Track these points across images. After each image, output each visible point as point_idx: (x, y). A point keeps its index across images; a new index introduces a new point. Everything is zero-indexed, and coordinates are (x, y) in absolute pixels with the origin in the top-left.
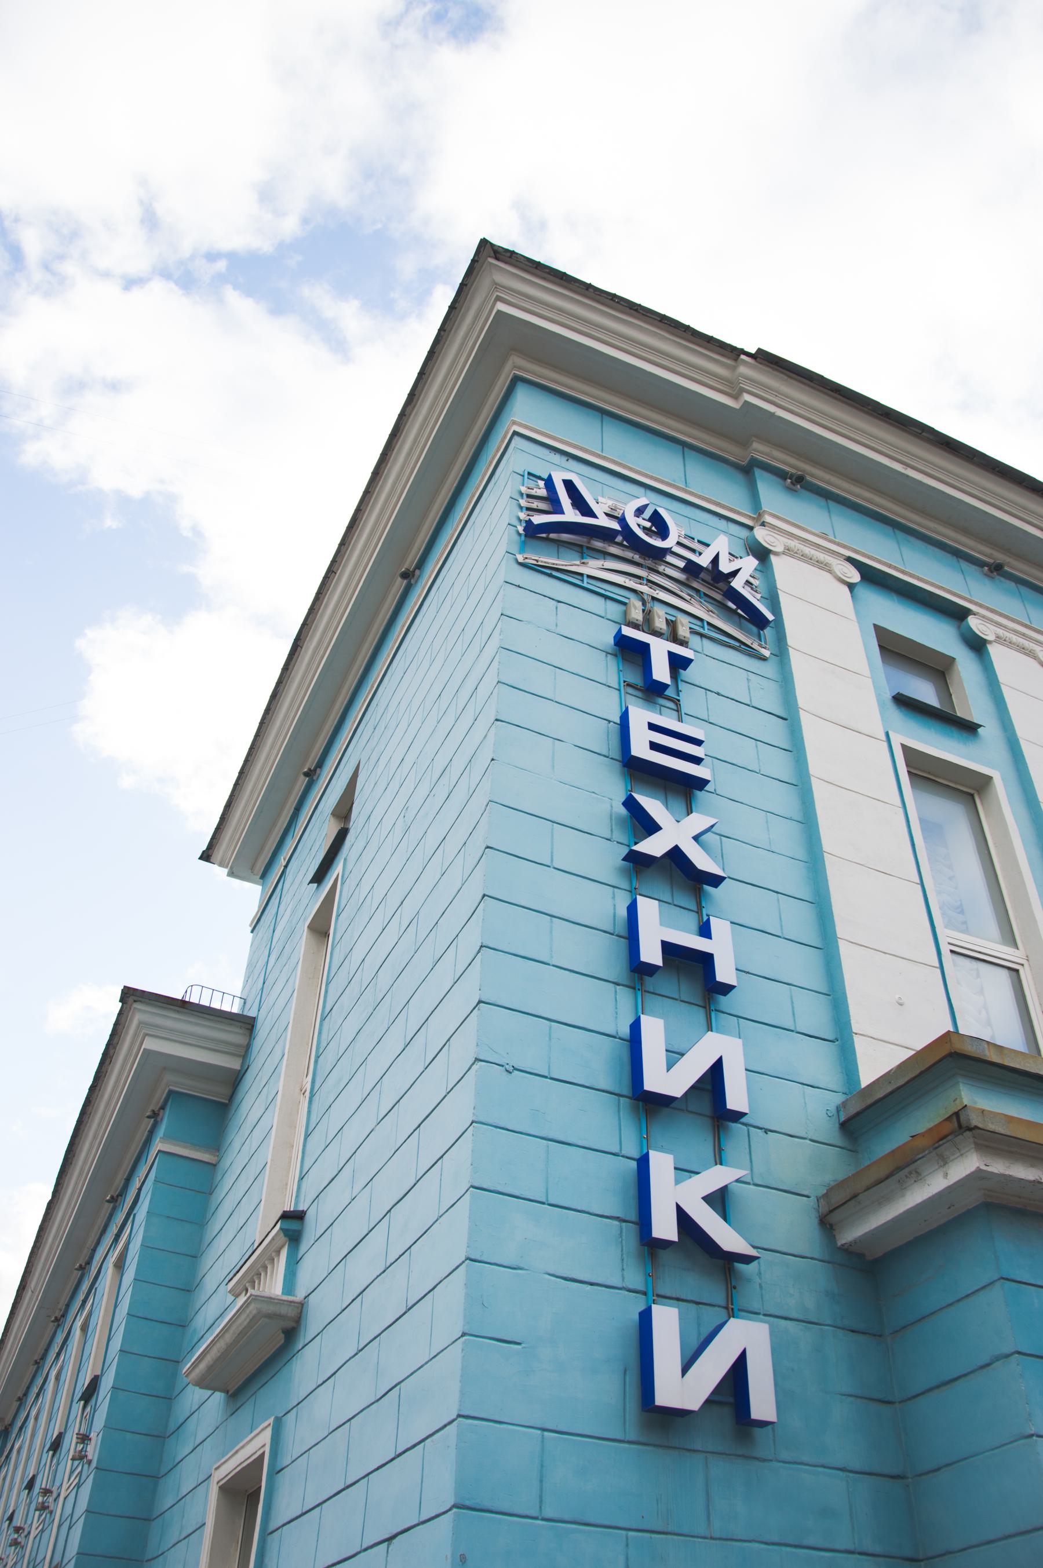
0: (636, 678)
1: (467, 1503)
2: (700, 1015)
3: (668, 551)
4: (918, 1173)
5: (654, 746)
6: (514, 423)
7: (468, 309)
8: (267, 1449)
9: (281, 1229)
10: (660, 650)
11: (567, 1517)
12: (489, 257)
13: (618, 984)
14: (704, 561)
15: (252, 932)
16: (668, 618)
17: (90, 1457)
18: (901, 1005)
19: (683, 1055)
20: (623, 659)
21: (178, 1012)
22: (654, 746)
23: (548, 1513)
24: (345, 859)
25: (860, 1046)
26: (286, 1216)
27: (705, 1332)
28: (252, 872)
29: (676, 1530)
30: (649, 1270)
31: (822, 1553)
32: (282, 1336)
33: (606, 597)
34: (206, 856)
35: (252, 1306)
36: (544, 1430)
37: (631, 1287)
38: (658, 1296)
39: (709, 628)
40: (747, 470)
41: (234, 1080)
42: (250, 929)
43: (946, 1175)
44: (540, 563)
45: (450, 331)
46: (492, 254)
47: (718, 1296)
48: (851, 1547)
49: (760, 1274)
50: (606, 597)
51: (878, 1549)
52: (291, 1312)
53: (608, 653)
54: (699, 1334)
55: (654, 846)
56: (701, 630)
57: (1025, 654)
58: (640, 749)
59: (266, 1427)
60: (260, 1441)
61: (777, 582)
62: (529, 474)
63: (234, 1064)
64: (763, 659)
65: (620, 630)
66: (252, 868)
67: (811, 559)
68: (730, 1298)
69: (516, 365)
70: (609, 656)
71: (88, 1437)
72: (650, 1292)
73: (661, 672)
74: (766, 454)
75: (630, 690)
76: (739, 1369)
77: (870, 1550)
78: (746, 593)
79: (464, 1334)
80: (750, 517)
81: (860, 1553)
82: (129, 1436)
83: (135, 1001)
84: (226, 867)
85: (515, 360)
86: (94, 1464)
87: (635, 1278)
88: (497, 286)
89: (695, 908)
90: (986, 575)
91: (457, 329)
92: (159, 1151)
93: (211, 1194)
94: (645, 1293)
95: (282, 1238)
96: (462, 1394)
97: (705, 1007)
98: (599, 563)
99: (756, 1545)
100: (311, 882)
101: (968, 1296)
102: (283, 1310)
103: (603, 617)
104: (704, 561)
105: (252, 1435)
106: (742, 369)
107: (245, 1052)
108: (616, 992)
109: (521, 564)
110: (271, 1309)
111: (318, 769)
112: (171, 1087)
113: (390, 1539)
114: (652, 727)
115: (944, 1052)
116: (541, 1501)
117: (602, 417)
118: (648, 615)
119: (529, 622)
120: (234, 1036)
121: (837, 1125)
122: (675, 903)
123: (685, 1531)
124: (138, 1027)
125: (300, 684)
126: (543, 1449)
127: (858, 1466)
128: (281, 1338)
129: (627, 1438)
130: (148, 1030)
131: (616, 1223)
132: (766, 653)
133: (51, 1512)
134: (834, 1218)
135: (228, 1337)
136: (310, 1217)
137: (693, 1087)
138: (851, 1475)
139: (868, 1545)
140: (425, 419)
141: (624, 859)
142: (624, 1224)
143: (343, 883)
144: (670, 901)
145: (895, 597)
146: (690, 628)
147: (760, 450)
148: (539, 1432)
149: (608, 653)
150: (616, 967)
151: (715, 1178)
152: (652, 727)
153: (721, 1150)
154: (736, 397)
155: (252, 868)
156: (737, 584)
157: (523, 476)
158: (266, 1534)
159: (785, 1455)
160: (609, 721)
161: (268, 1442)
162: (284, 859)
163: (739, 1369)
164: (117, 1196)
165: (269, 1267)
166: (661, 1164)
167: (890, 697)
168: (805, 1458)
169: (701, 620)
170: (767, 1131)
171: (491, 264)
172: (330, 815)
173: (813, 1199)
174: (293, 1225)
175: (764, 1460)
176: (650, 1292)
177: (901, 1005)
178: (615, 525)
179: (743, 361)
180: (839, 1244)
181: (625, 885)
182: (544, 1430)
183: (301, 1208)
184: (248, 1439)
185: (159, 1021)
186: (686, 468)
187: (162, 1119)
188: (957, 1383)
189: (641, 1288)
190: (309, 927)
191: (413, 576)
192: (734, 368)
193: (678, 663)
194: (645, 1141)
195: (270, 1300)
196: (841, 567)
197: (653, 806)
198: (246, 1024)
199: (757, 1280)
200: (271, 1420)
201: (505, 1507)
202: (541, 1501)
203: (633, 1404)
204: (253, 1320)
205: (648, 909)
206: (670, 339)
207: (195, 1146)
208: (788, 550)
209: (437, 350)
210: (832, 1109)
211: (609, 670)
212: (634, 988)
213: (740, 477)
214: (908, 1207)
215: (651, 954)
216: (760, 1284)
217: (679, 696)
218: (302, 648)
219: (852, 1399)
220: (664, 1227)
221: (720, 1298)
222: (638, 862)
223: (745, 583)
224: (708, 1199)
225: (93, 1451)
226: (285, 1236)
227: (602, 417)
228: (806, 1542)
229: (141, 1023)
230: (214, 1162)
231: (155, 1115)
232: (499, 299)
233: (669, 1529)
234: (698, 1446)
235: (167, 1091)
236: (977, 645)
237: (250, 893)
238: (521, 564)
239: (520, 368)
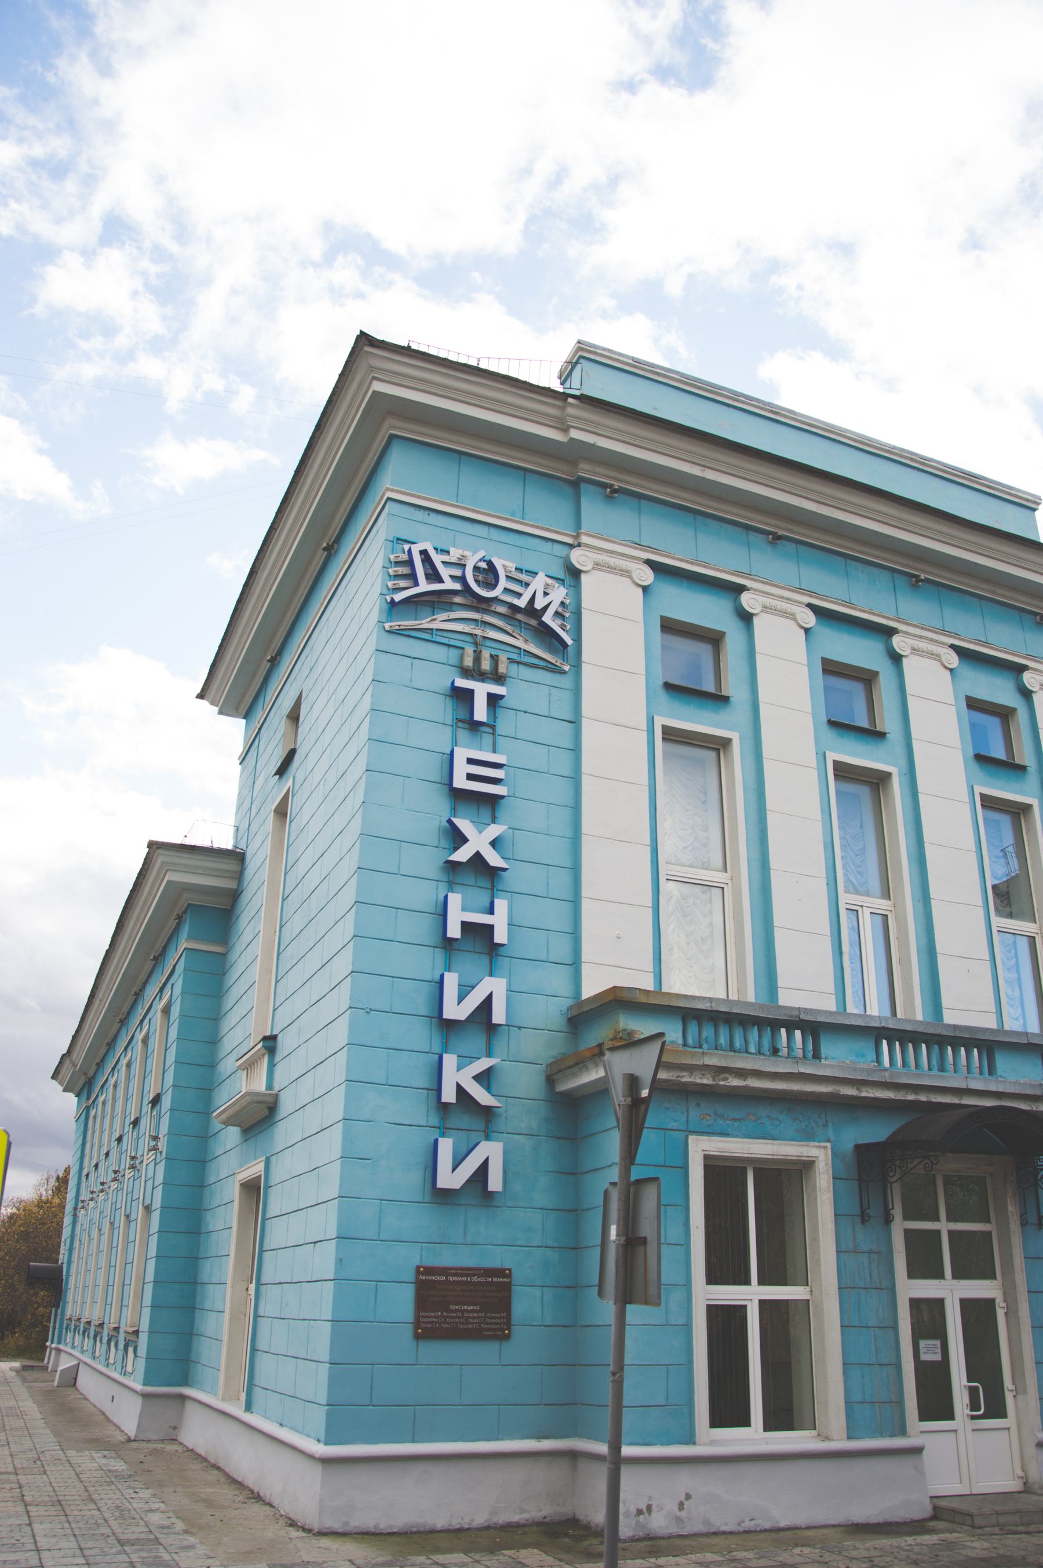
0: (463, 715)
1: (343, 1236)
2: (485, 959)
3: (495, 599)
4: (587, 1068)
5: (470, 777)
6: (388, 489)
7: (353, 379)
8: (263, 1173)
9: (263, 1046)
10: (481, 690)
11: (392, 1239)
12: (366, 345)
13: (436, 947)
14: (522, 603)
15: (241, 764)
16: (493, 653)
17: (161, 1150)
18: (619, 938)
19: (473, 987)
20: (457, 698)
21: (189, 853)
22: (470, 777)
23: (382, 1237)
24: (294, 777)
25: (586, 970)
26: (265, 1039)
27: (471, 1145)
28: (237, 712)
29: (447, 1242)
30: (442, 1116)
31: (524, 1248)
32: (267, 1110)
33: (449, 646)
34: (201, 696)
35: (248, 1097)
36: (382, 1200)
37: (432, 1125)
38: (446, 1128)
39: (525, 653)
40: (576, 484)
41: (234, 896)
42: (238, 762)
43: (597, 1072)
44: (402, 627)
45: (342, 388)
46: (367, 343)
47: (481, 1126)
48: (541, 1244)
49: (506, 1111)
50: (449, 646)
51: (555, 1245)
52: (271, 1100)
53: (446, 695)
54: (468, 1147)
55: (463, 855)
56: (519, 659)
57: (787, 617)
58: (460, 782)
59: (261, 1162)
60: (257, 1168)
61: (583, 602)
62: (398, 539)
63: (231, 885)
64: (564, 672)
65: (453, 683)
66: (237, 709)
67: (615, 569)
68: (487, 1127)
69: (392, 426)
70: (447, 697)
71: (157, 1137)
72: (442, 1128)
73: (481, 713)
74: (590, 471)
75: (460, 724)
76: (484, 1166)
77: (551, 1245)
78: (555, 625)
79: (341, 1158)
80: (571, 535)
81: (545, 1247)
82: (184, 1138)
83: (158, 848)
84: (217, 706)
85: (391, 421)
86: (164, 1155)
87: (434, 1120)
88: (372, 368)
89: (490, 886)
90: (770, 542)
91: (347, 390)
92: (185, 949)
93: (224, 975)
94: (439, 1128)
95: (264, 1051)
96: (341, 1186)
97: (489, 954)
98: (444, 616)
99: (489, 1246)
100: (275, 774)
101: (608, 1130)
102: (267, 1099)
103: (445, 664)
104: (522, 603)
105: (254, 1163)
106: (570, 410)
107: (240, 876)
108: (434, 953)
109: (388, 631)
110: (259, 1098)
111: (278, 657)
112: (189, 902)
113: (315, 1243)
114: (471, 761)
115: (611, 998)
116: (379, 1233)
117: (460, 458)
118: (477, 659)
119: (392, 683)
120: (232, 866)
121: (566, 1019)
122: (478, 885)
123: (452, 1242)
124: (162, 864)
125: (258, 597)
126: (381, 1209)
127: (550, 1207)
128: (266, 1112)
129: (425, 1201)
130: (169, 867)
131: (426, 1091)
132: (567, 668)
133: (139, 1170)
134: (555, 1077)
135: (237, 1107)
136: (279, 1038)
137: (478, 1007)
138: (546, 1211)
139: (550, 1243)
140: (330, 445)
141: (444, 863)
142: (430, 1092)
143: (293, 796)
144: (474, 884)
145: (685, 582)
146: (508, 659)
147: (585, 470)
148: (379, 1201)
149: (446, 695)
150: (434, 939)
151: (483, 1064)
152: (471, 761)
153: (490, 1043)
154: (565, 430)
155: (237, 709)
156: (547, 618)
157: (393, 542)
158: (264, 1220)
159: (510, 1204)
160: (444, 754)
161: (263, 1169)
162: (258, 723)
163: (484, 1166)
164: (158, 956)
165: (259, 1062)
166: (450, 1061)
167: (662, 683)
168: (521, 1205)
169: (520, 649)
170: (520, 1028)
171: (366, 352)
172: (285, 717)
173: (544, 1065)
174: (270, 1043)
175: (498, 1207)
176: (442, 1128)
177: (619, 938)
178: (457, 586)
179: (570, 403)
180: (557, 1090)
181: (445, 879)
182: (382, 1200)
183: (274, 1033)
184: (252, 1164)
185: (176, 860)
186: (526, 493)
187: (185, 920)
188: (600, 1171)
189: (438, 1125)
190: (275, 811)
191: (333, 549)
192: (563, 408)
193: (493, 700)
194: (445, 1044)
195: (258, 1094)
196: (639, 571)
197: (464, 825)
198: (237, 857)
199: (505, 1114)
200: (264, 1158)
201: (362, 1236)
202: (379, 1233)
203: (428, 1185)
204: (249, 1104)
205: (455, 900)
206: (510, 392)
207: (209, 942)
208: (597, 565)
209: (334, 399)
210: (564, 1009)
211: (444, 710)
212: (446, 948)
213: (568, 490)
214: (584, 1082)
215: (454, 931)
216: (506, 1117)
217: (495, 722)
218: (257, 573)
219: (551, 1174)
220: (449, 1095)
221: (482, 1127)
222: (453, 867)
223: (554, 615)
224: (477, 1078)
225: (162, 1145)
226: (266, 1049)
227: (460, 458)
228: (516, 1244)
229: (163, 863)
230: (224, 952)
231: (180, 918)
232: (374, 378)
233: (444, 1242)
234: (462, 1202)
235: (186, 905)
236: (746, 618)
237: (235, 729)
238: (388, 631)
239: (395, 428)
